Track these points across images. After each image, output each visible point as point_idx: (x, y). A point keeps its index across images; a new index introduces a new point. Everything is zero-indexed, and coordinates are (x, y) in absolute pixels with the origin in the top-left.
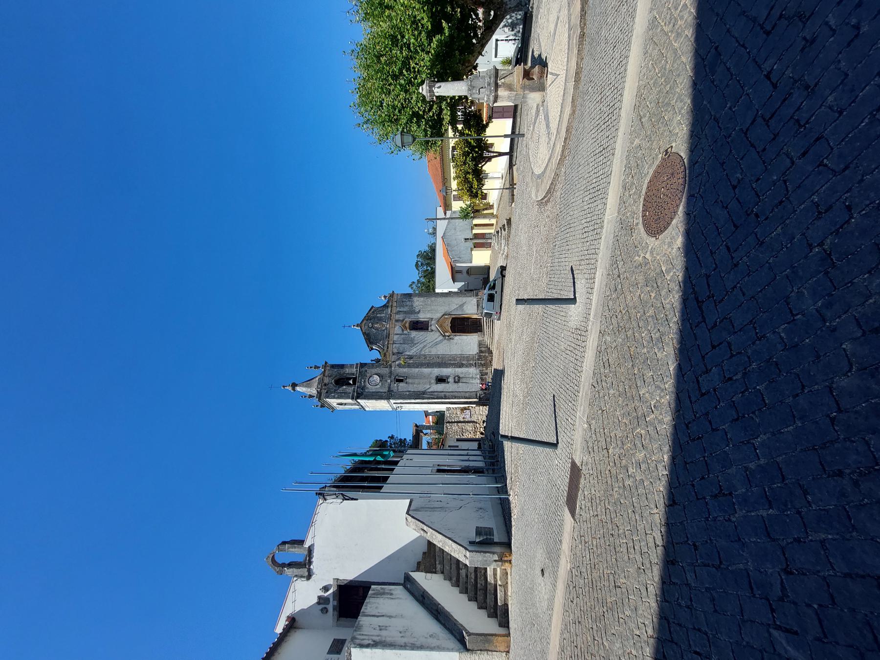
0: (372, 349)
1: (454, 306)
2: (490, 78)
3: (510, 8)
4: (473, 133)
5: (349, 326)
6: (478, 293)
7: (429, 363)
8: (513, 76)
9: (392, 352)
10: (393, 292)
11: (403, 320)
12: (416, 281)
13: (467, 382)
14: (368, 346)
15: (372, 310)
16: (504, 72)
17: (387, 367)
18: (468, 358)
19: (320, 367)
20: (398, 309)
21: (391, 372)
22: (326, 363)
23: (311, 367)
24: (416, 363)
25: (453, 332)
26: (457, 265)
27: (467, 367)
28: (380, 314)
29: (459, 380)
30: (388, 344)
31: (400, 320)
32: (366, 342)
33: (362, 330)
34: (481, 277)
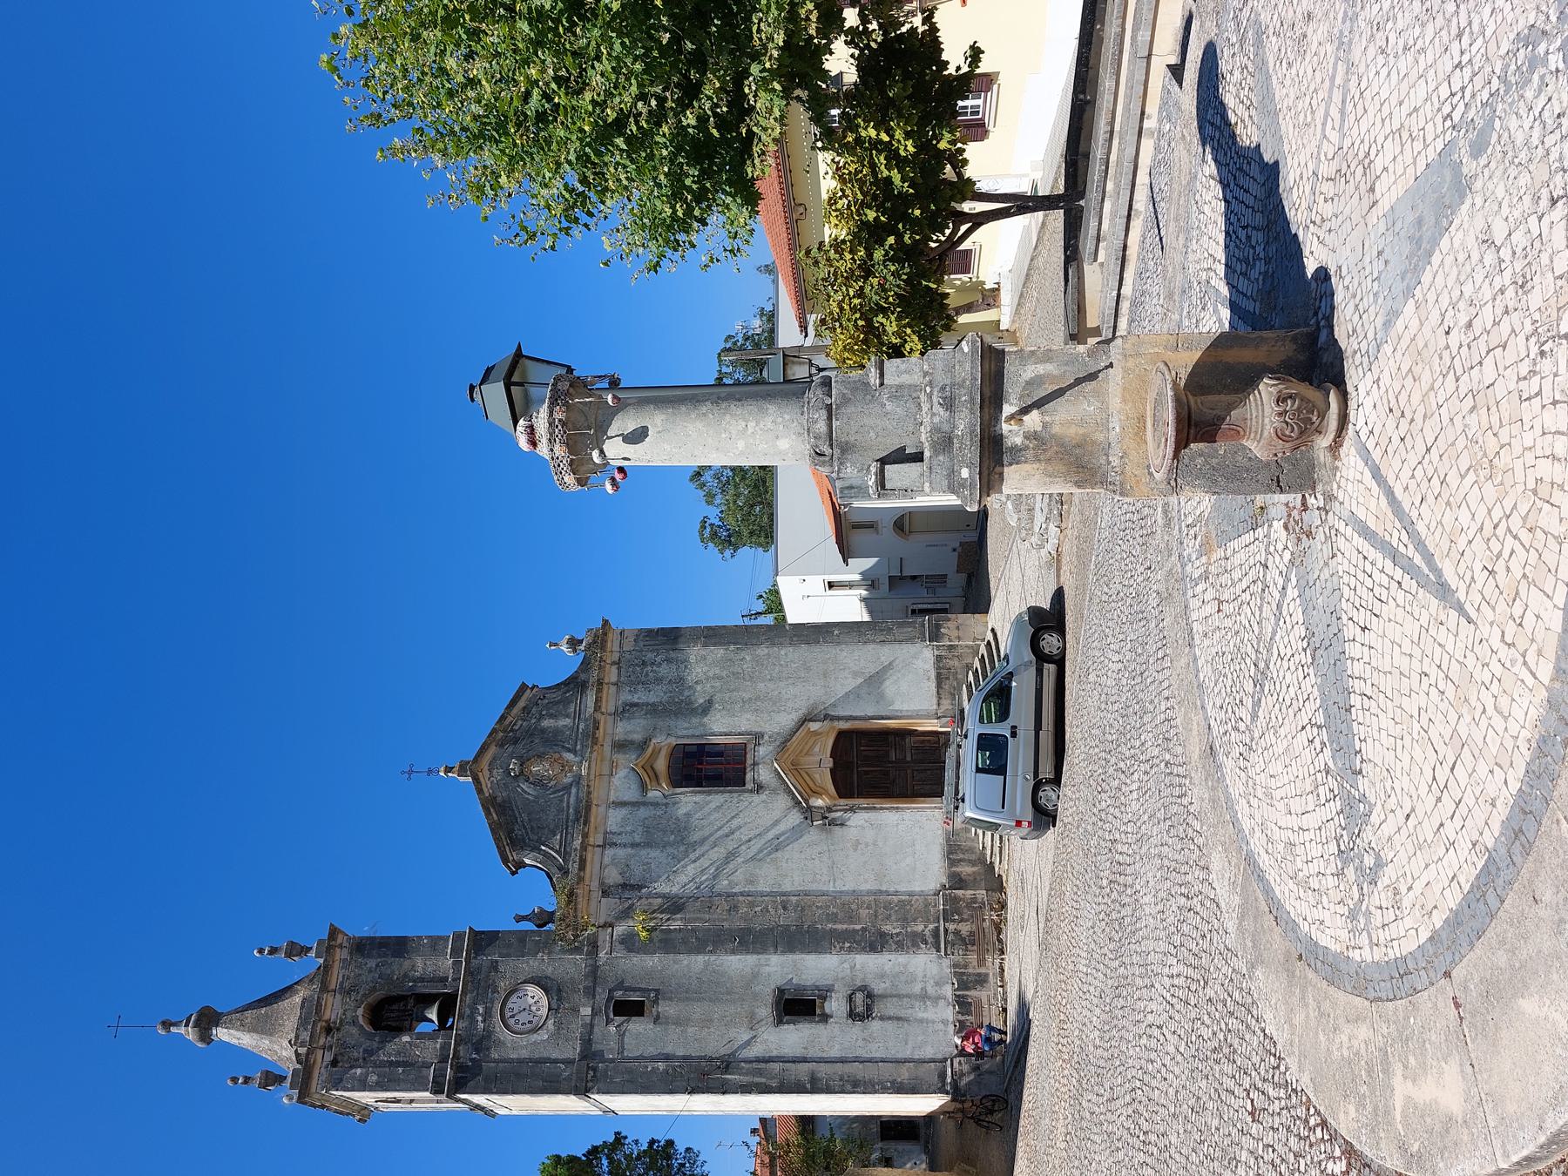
2: (949, 404)
4: (899, 134)
6: (938, 627)
7: (749, 931)
8: (1098, 394)
9: (602, 883)
10: (606, 623)
11: (645, 743)
13: (902, 1013)
14: (505, 860)
15: (522, 704)
16: (1041, 369)
17: (578, 950)
18: (903, 908)
20: (626, 697)
21: (594, 973)
22: (334, 932)
23: (273, 951)
26: (856, 504)
27: (900, 947)
28: (552, 716)
29: (869, 1008)
30: (584, 847)
31: (632, 742)
32: (497, 840)
33: (480, 791)
34: (954, 540)
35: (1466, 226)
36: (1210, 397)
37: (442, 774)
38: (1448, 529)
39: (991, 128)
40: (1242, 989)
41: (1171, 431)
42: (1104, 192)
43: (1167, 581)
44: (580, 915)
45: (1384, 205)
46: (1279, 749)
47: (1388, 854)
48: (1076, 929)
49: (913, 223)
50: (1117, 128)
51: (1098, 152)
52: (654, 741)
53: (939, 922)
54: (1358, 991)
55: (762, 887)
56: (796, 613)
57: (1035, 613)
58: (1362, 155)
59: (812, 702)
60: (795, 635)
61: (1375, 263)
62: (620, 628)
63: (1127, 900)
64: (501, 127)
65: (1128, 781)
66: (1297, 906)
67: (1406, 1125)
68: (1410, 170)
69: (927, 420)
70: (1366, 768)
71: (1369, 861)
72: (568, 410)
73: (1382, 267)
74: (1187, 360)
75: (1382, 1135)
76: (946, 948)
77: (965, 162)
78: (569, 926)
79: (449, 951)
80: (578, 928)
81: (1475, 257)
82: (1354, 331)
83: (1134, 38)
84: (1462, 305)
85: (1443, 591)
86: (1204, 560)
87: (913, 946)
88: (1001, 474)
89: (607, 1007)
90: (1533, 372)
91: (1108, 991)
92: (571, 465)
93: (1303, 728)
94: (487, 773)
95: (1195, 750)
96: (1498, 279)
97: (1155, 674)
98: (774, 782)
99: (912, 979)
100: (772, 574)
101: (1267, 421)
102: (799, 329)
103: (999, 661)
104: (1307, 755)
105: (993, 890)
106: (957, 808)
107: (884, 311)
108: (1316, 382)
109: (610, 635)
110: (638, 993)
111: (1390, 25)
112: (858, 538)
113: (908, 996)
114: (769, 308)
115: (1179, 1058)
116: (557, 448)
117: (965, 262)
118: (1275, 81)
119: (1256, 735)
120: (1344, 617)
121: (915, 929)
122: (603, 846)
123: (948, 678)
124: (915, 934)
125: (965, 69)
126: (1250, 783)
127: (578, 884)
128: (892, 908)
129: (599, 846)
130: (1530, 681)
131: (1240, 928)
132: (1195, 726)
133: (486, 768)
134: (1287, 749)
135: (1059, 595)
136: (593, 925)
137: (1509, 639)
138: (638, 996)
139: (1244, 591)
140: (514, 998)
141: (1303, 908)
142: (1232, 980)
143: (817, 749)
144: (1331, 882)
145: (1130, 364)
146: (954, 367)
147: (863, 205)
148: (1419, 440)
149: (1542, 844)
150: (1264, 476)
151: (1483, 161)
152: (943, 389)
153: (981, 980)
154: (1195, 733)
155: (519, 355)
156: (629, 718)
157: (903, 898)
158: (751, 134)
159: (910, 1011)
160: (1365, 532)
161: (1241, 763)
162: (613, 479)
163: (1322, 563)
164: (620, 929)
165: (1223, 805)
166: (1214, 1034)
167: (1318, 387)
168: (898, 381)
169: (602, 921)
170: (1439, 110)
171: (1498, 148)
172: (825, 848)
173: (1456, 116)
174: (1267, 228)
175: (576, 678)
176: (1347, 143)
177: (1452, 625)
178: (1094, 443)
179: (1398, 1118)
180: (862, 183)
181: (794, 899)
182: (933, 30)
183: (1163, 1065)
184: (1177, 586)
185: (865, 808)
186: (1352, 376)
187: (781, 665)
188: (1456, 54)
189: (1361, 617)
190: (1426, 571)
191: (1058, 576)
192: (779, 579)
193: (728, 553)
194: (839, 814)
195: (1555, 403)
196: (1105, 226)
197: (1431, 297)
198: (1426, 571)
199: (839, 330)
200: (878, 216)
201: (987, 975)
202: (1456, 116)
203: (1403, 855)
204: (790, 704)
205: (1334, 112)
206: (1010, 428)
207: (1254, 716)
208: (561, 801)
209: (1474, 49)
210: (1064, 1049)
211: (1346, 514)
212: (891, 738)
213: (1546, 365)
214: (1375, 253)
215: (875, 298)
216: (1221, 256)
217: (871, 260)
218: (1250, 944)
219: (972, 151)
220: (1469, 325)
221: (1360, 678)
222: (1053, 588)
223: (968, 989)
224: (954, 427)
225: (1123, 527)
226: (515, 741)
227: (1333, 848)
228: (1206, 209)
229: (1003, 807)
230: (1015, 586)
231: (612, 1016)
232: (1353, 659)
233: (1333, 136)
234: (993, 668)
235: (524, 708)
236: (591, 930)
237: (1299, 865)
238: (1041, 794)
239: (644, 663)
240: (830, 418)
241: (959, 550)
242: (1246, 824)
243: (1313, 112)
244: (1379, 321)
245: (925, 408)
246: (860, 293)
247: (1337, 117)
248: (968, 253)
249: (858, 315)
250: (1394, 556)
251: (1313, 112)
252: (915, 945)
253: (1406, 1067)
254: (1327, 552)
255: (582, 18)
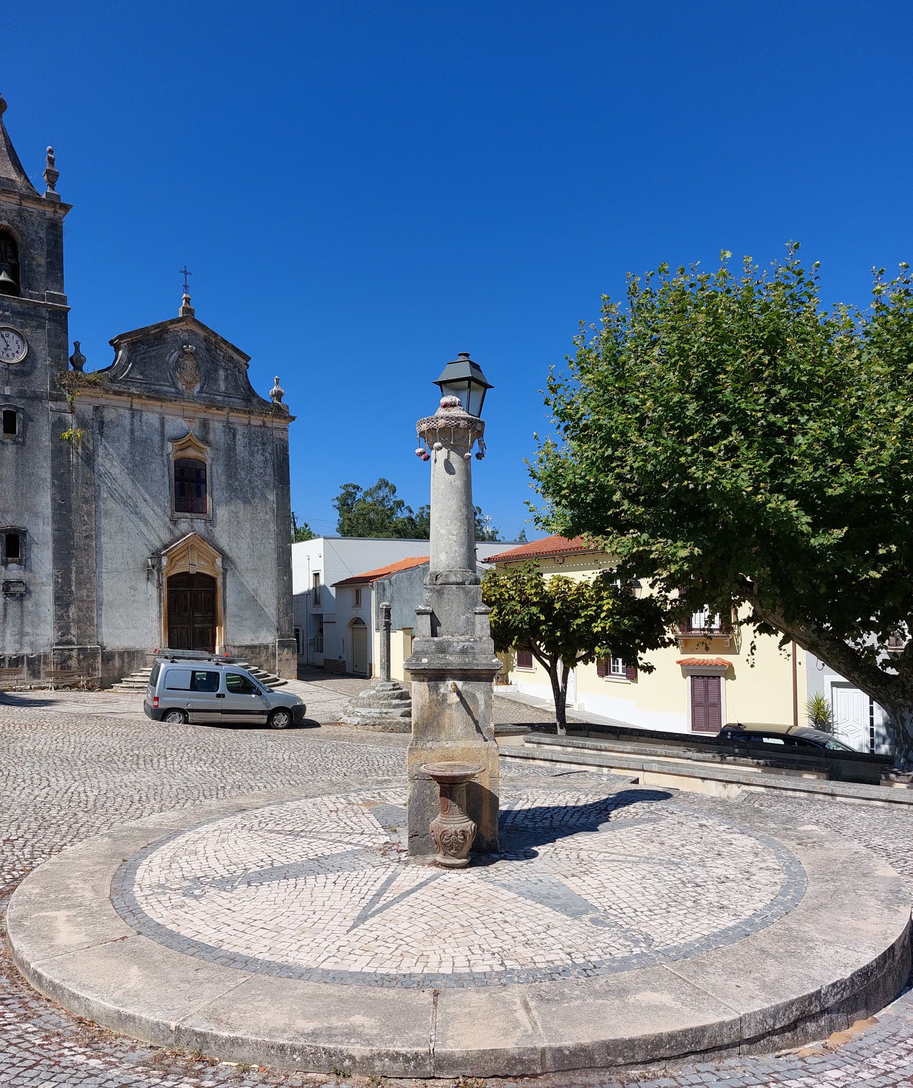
0: (117, 348)
1: (251, 582)
2: (464, 651)
3: (903, 720)
5: (186, 287)
6: (288, 647)
7: (69, 511)
8: (467, 735)
9: (104, 407)
10: (293, 419)
11: (207, 442)
12: (399, 496)
13: (9, 619)
14: (121, 337)
15: (236, 356)
16: (482, 702)
17: (53, 386)
18: (88, 620)
19: (53, 188)
20: (240, 430)
21: (36, 398)
22: (66, 207)
23: (51, 161)
24: (69, 472)
25: (168, 578)
26: (373, 593)
27: (59, 618)
28: (226, 377)
29: (12, 595)
30: (131, 395)
31: (207, 433)
32: (136, 332)
33: (172, 322)
34: (347, 658)
35: (556, 918)
36: (465, 795)
37: (184, 296)
38: (397, 918)
39: (605, 678)
40: (88, 832)
41: (448, 773)
42: (566, 746)
43: (344, 783)
44: (81, 389)
45: (565, 882)
46: (253, 844)
47: (203, 901)
48: (98, 734)
49: (552, 631)
50: (603, 753)
51: (589, 743)
52: (208, 448)
53: (78, 645)
54: (113, 891)
55: (105, 523)
56: (297, 549)
57: (302, 709)
58: (591, 870)
59: (236, 560)
60: (283, 550)
61: (535, 878)
62: (289, 428)
63: (128, 765)
64: (620, 377)
65: (207, 765)
66: (160, 856)
67: (38, 918)
68: (584, 892)
69: (455, 639)
70: (253, 888)
71: (197, 892)
72: (464, 429)
73: (533, 882)
74: (484, 781)
75: (27, 907)
76: (59, 649)
77: (586, 663)
78: (72, 380)
79: (52, 292)
80: (70, 388)
81: (541, 923)
82: (499, 870)
83: (654, 761)
84: (516, 918)
85: (363, 918)
86: (360, 802)
87: (60, 627)
88: (423, 681)
89: (10, 406)
90: (483, 951)
91: (62, 754)
92: (433, 429)
93: (270, 856)
94: (185, 328)
95: (241, 801)
96: (530, 933)
97: (279, 780)
98: (177, 533)
99: (35, 626)
100: (326, 535)
101: (452, 825)
102: (487, 558)
103: (269, 686)
104: (253, 859)
105: (101, 682)
106: (166, 658)
107: (500, 613)
108: (471, 853)
109: (284, 421)
110: (21, 429)
111: (657, 880)
112: (350, 594)
113: (22, 623)
114: (498, 537)
115: (32, 797)
116: (443, 421)
117: (525, 663)
118: (629, 828)
119: (260, 833)
120: (339, 874)
121: (72, 628)
122: (131, 409)
123: (252, 653)
124: (68, 628)
125: (640, 663)
126: (228, 831)
127: (104, 389)
128: (88, 613)
129: (132, 406)
130: (320, 960)
131: (132, 829)
132: (256, 801)
133: (189, 328)
134: (254, 849)
135: (314, 724)
136: (73, 399)
137: (341, 949)
138: (19, 429)
139: (345, 823)
140: (16, 338)
141: (157, 860)
142: (92, 826)
143: (203, 563)
144: (179, 874)
145: (483, 752)
146: (484, 654)
147: (564, 600)
148: (443, 903)
149: (230, 971)
150: (418, 827)
151: (588, 923)
152: (472, 648)
153: (35, 674)
154: (252, 801)
155: (487, 386)
156: (224, 432)
157: (95, 621)
158: (609, 534)
159: (11, 624)
160: (390, 881)
161: (240, 826)
162: (424, 453)
163: (369, 861)
164: (69, 417)
165: (210, 817)
166: (54, 817)
167: (468, 855)
168: (477, 622)
169: (76, 405)
170: (614, 904)
171: (595, 930)
172: (131, 567)
173: (611, 911)
174: (552, 827)
175: (254, 396)
176: (597, 863)
177: (344, 923)
178: (440, 732)
179: (41, 914)
180: (578, 600)
181: (94, 544)
182: (666, 645)
183: (24, 788)
184: (342, 788)
185: (160, 595)
186: (475, 871)
187: (262, 540)
188: (641, 910)
189: (341, 881)
190: (372, 910)
191: (326, 724)
192: (321, 541)
193: (337, 503)
194: (156, 577)
195: (469, 961)
196: (546, 747)
197: (519, 905)
198: (372, 910)
199: (489, 585)
200: (556, 610)
201: (39, 678)
202: (611, 911)
203: (205, 908)
204: (234, 545)
205: (613, 857)
206: (450, 686)
207: (271, 831)
208: (165, 381)
209: (644, 917)
210: (11, 728)
211: (399, 872)
212: (210, 614)
213: (487, 955)
214: (540, 878)
215: (508, 608)
216: (536, 805)
217: (531, 606)
218: (124, 834)
219: (593, 666)
220: (506, 922)
221: (305, 882)
222: (318, 721)
223: (28, 665)
224: (451, 654)
225: (369, 759)
226: (208, 350)
227: (199, 874)
228: (561, 797)
229: (168, 689)
230: (317, 697)
231: (4, 409)
232: (316, 878)
233: (601, 857)
234: (265, 682)
235: (232, 358)
236: (69, 397)
237: (184, 858)
238: (177, 714)
239: (264, 444)
240: (458, 584)
241: (340, 661)
242: (202, 829)
243: (613, 847)
244: (505, 882)
245: (462, 638)
246: (511, 598)
247: (610, 858)
248: (529, 664)
249: (498, 597)
250: (379, 895)
251: (613, 847)
252: (60, 629)
253: (75, 916)
254: (375, 863)
255: (679, 435)
